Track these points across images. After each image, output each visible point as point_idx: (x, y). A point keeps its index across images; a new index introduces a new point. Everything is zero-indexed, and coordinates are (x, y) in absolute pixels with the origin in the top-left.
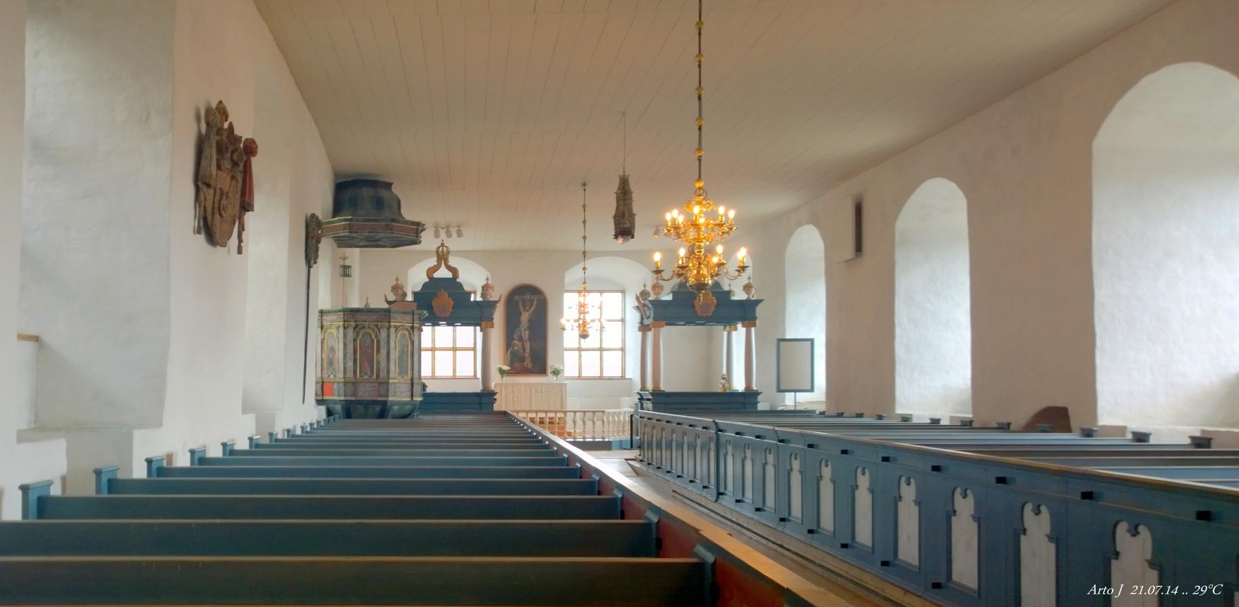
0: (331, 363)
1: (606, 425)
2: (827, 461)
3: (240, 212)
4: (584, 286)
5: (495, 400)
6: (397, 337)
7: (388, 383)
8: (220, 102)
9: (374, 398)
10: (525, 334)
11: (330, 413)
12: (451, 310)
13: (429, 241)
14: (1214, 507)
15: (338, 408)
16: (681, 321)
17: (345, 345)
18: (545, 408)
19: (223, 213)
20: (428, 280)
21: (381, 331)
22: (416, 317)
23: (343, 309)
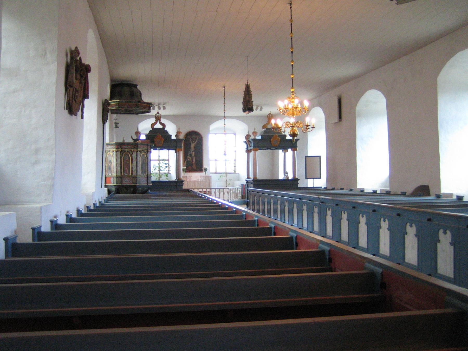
1: (229, 194)
2: (316, 206)
3: (83, 99)
4: (225, 132)
5: (183, 184)
6: (140, 156)
7: (137, 177)
8: (76, 48)
9: (130, 184)
10: (193, 153)
11: (109, 192)
13: (153, 112)
14: (376, 209)
15: (113, 189)
18: (202, 187)
19: (76, 100)
20: (152, 129)
22: (149, 146)
23: (116, 143)
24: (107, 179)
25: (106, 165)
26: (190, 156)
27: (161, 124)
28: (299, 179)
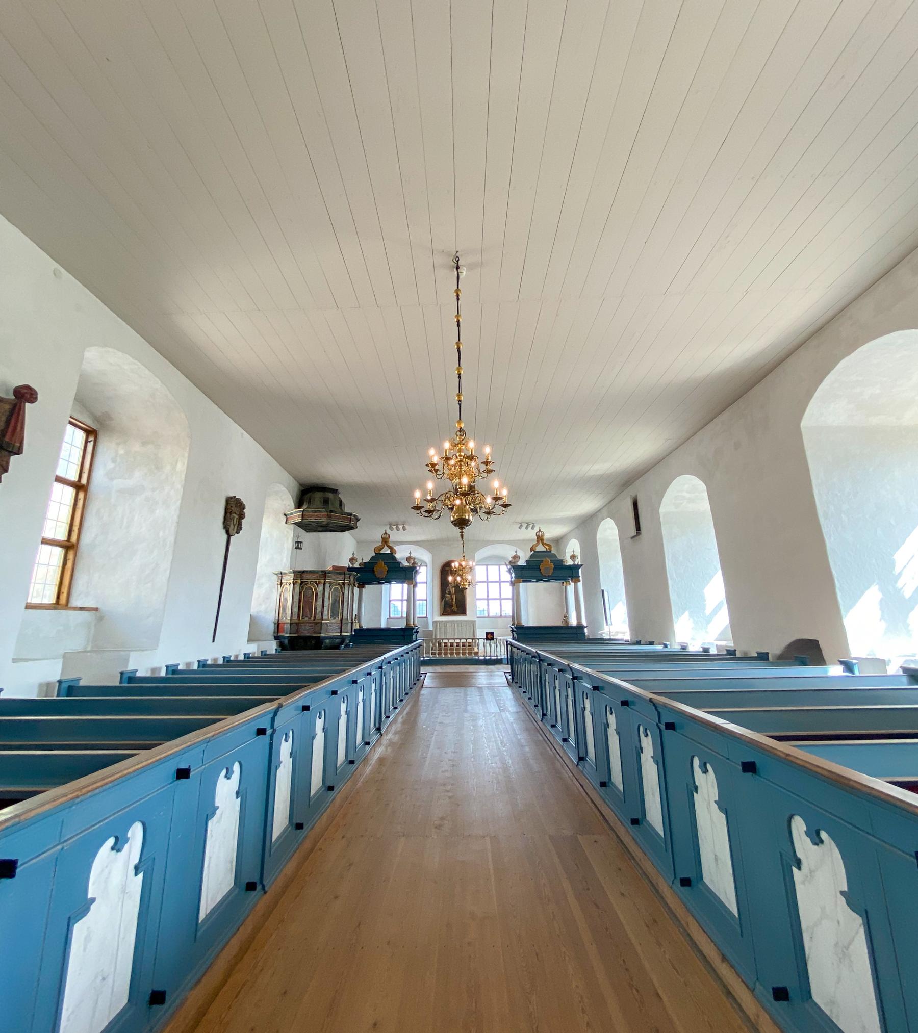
6: (331, 590)
12: (386, 573)
15: (286, 641)
16: (533, 579)
20: (374, 555)
21: (319, 586)
26: (449, 594)
27: (543, 544)
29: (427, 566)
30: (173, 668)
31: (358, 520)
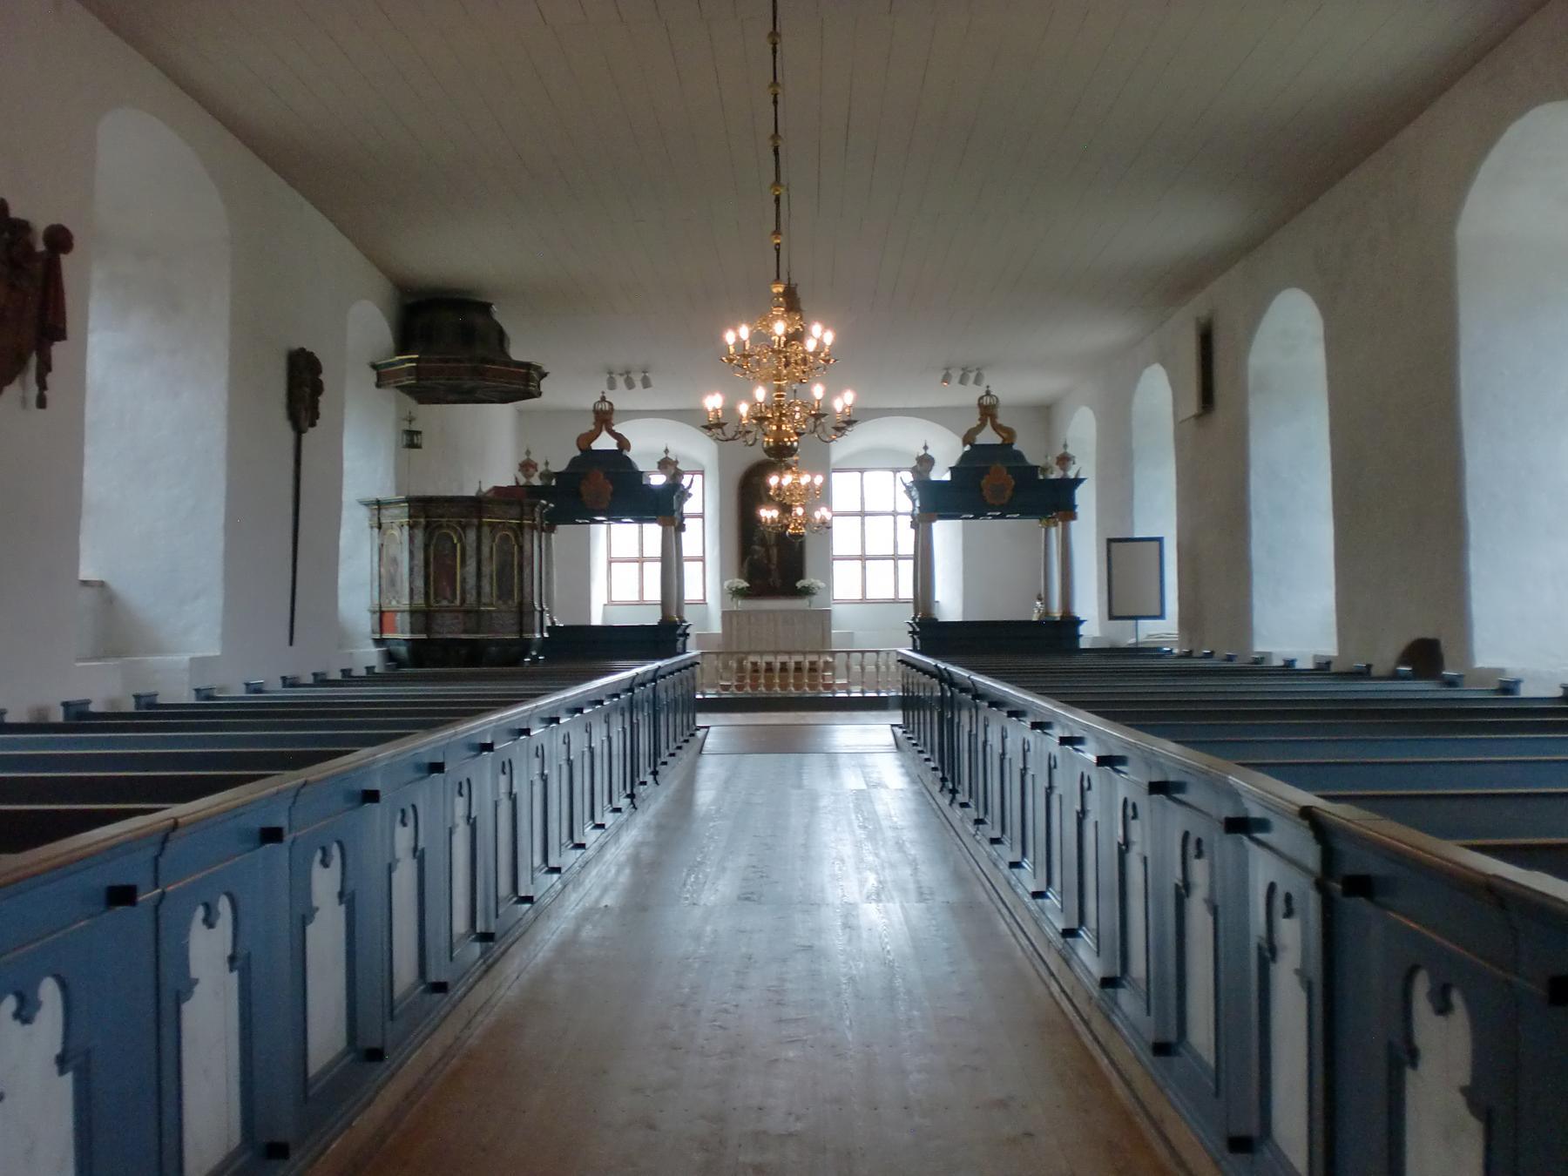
0: (393, 583)
6: (493, 541)
12: (609, 498)
15: (403, 650)
17: (411, 553)
20: (578, 453)
24: (386, 618)
25: (382, 570)
27: (997, 428)
28: (1082, 619)
29: (702, 473)
30: (147, 700)
31: (544, 375)
